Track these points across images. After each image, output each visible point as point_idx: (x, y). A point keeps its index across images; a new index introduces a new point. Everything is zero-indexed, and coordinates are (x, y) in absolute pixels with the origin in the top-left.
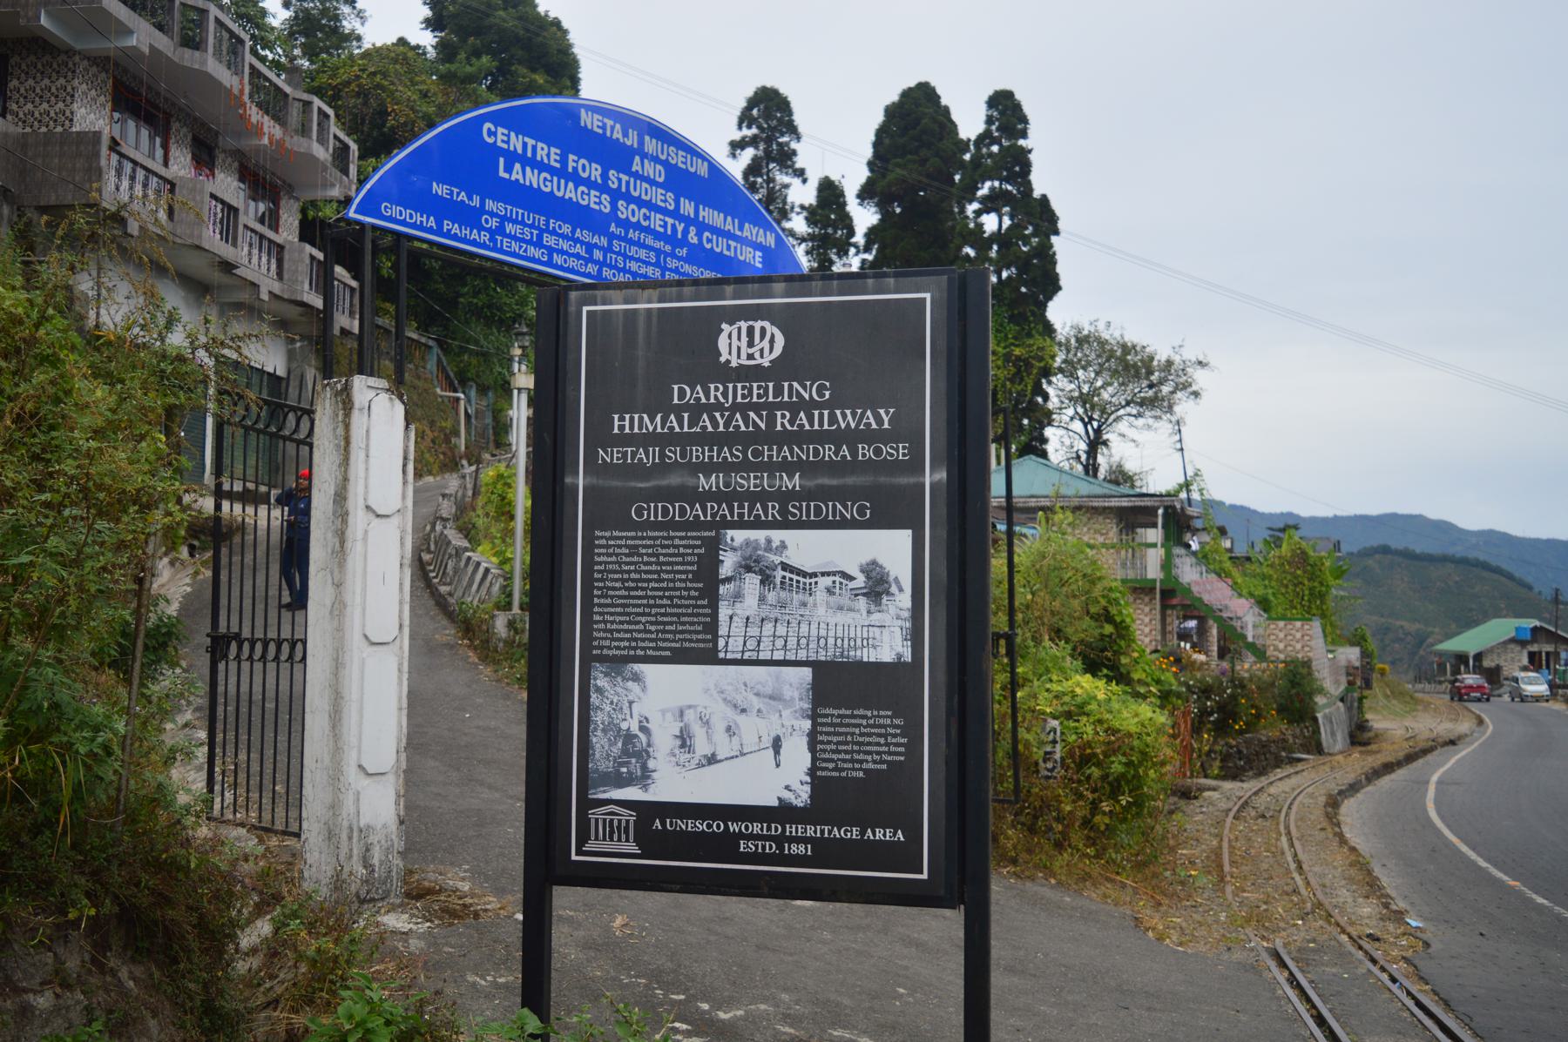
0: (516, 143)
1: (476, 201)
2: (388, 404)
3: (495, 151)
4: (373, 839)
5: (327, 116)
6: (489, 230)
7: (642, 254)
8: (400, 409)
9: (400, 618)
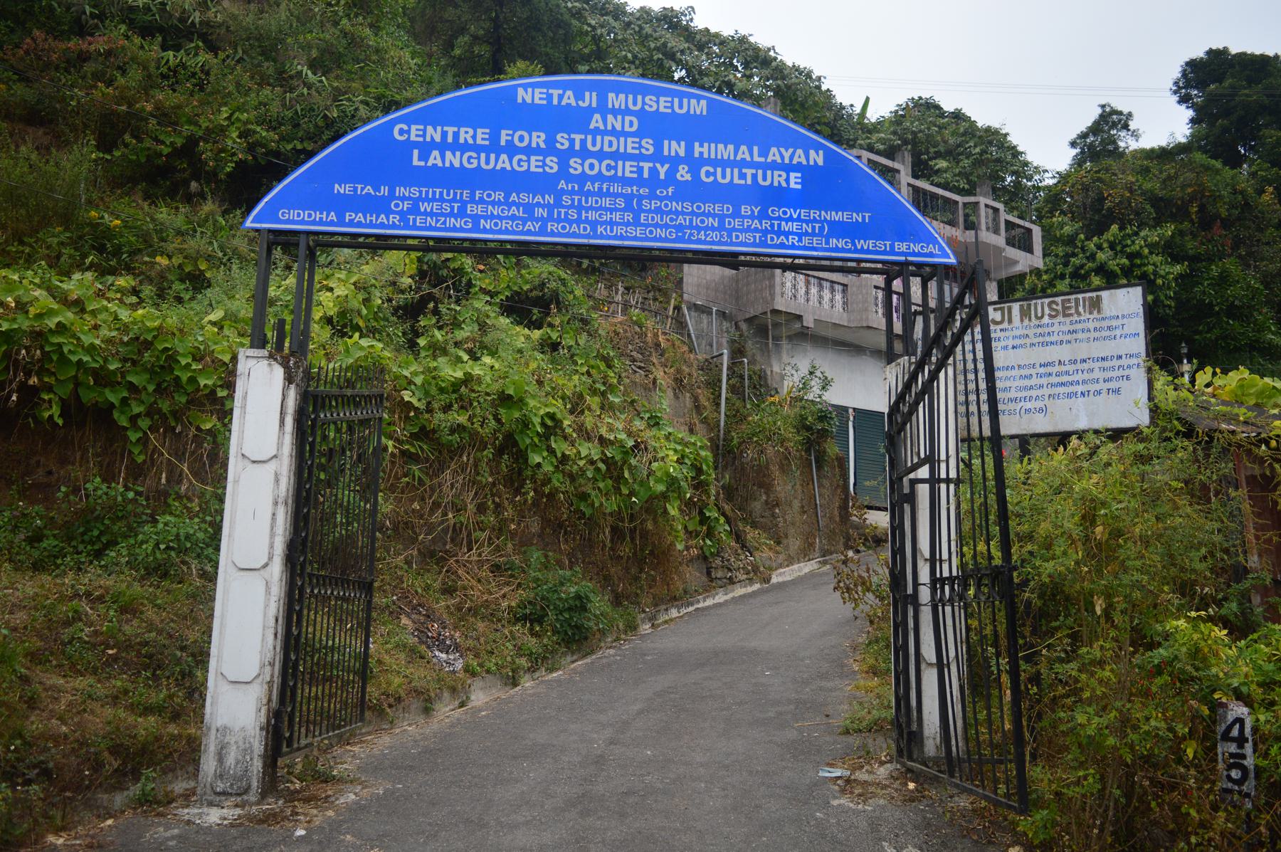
0: (434, 134)
1: (384, 191)
2: (266, 369)
3: (410, 145)
4: (231, 739)
5: (996, 210)
6: (401, 213)
7: (606, 202)
8: (279, 372)
9: (272, 546)
